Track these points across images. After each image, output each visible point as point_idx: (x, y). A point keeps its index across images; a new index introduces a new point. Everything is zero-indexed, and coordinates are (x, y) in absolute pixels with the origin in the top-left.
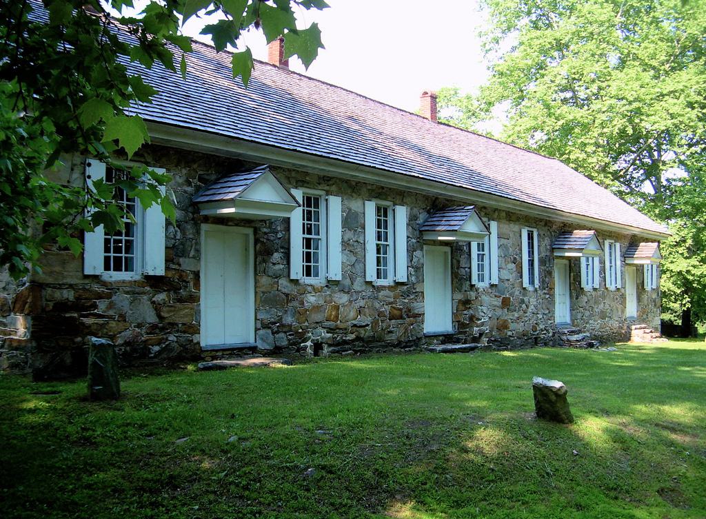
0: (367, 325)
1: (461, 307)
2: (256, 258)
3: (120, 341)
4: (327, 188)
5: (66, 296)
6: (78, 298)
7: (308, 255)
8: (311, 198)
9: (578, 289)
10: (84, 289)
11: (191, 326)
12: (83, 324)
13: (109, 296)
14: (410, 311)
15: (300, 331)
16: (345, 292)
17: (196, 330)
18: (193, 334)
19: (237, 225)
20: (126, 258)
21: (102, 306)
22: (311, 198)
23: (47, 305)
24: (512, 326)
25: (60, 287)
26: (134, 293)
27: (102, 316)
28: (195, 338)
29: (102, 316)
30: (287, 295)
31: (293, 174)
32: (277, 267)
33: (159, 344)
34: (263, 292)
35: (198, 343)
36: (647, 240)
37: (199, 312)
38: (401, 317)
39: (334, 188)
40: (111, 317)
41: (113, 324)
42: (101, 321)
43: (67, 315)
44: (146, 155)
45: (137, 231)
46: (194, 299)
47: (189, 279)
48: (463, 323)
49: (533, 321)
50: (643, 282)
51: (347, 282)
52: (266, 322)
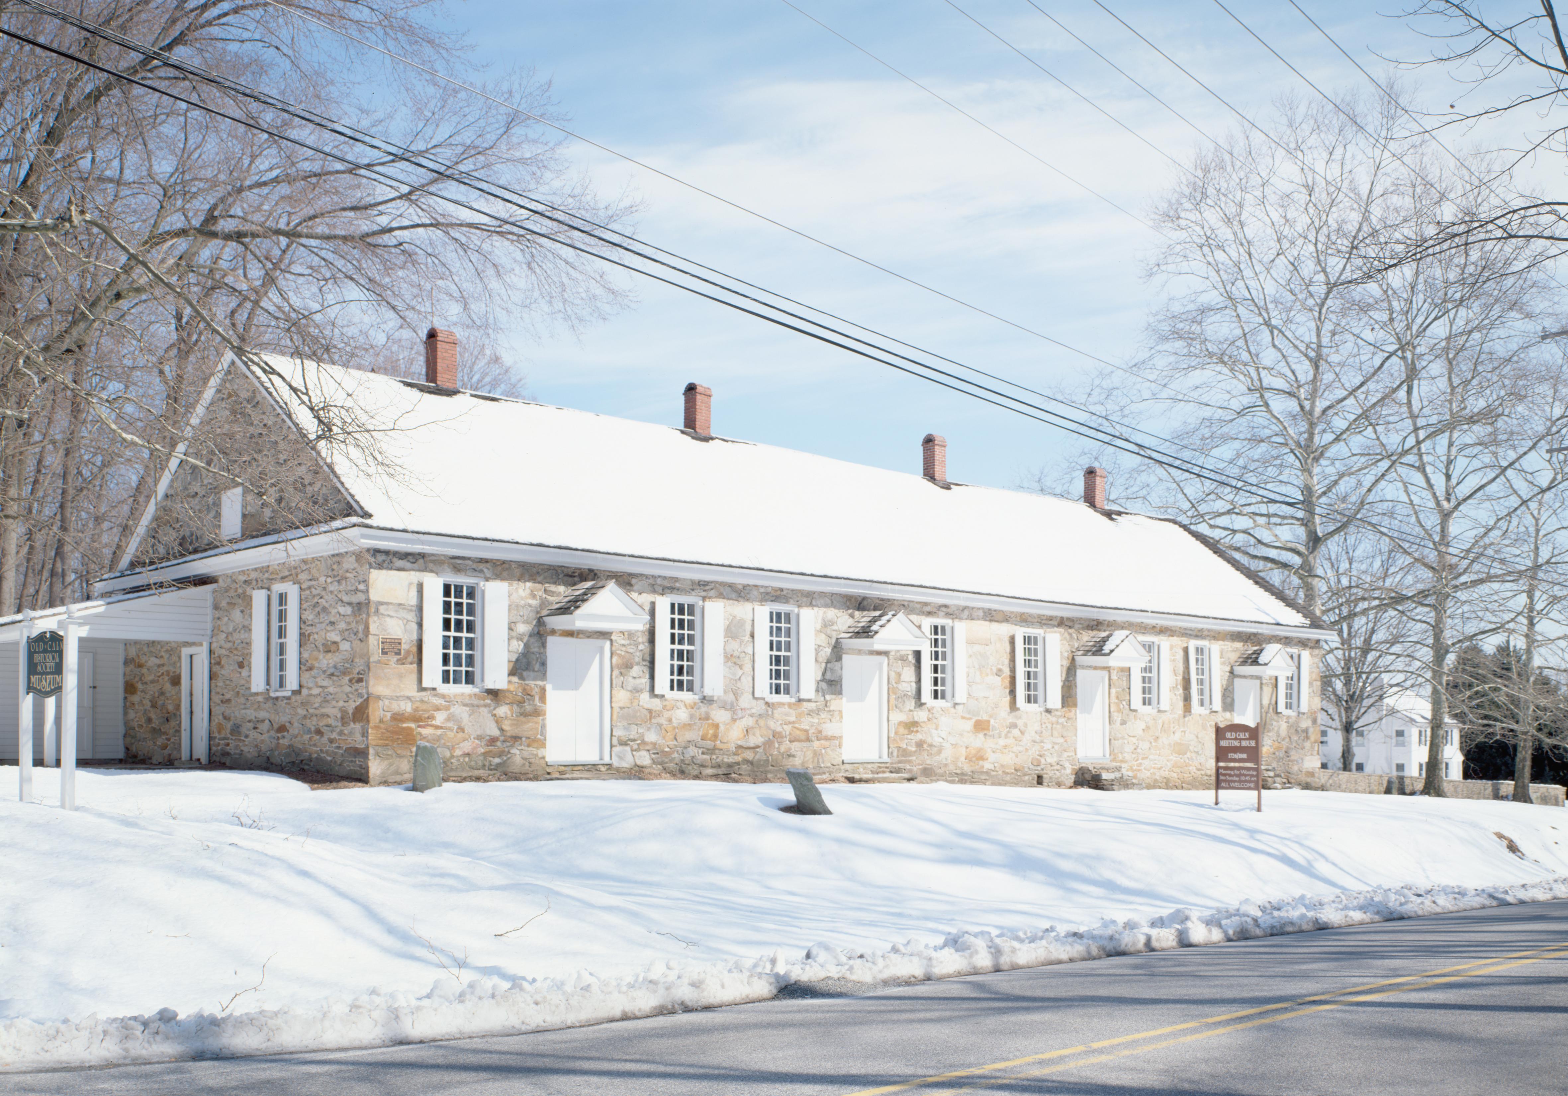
0: (758, 747)
1: (902, 730)
2: (612, 671)
3: (458, 752)
4: (704, 594)
5: (403, 707)
6: (416, 710)
7: (936, 679)
8: (462, 587)
9: (1127, 711)
10: (422, 701)
11: (535, 740)
12: (420, 734)
13: (447, 708)
14: (820, 732)
15: (667, 749)
16: (726, 710)
17: (542, 744)
18: (538, 748)
19: (589, 637)
20: (467, 672)
21: (440, 718)
22: (462, 587)
23: (385, 716)
24: (992, 757)
25: (397, 698)
26: (473, 705)
27: (441, 728)
28: (541, 752)
29: (441, 728)
30: (650, 711)
31: (659, 581)
32: (638, 681)
33: (500, 756)
34: (621, 708)
35: (544, 758)
36: (906, 607)
37: (544, 726)
38: (808, 740)
39: (712, 593)
40: (450, 729)
41: (451, 734)
42: (439, 732)
43: (405, 725)
44: (485, 570)
45: (478, 644)
46: (537, 713)
47: (533, 693)
48: (905, 750)
49: (1034, 751)
50: (1276, 703)
51: (731, 697)
52: (624, 739)
